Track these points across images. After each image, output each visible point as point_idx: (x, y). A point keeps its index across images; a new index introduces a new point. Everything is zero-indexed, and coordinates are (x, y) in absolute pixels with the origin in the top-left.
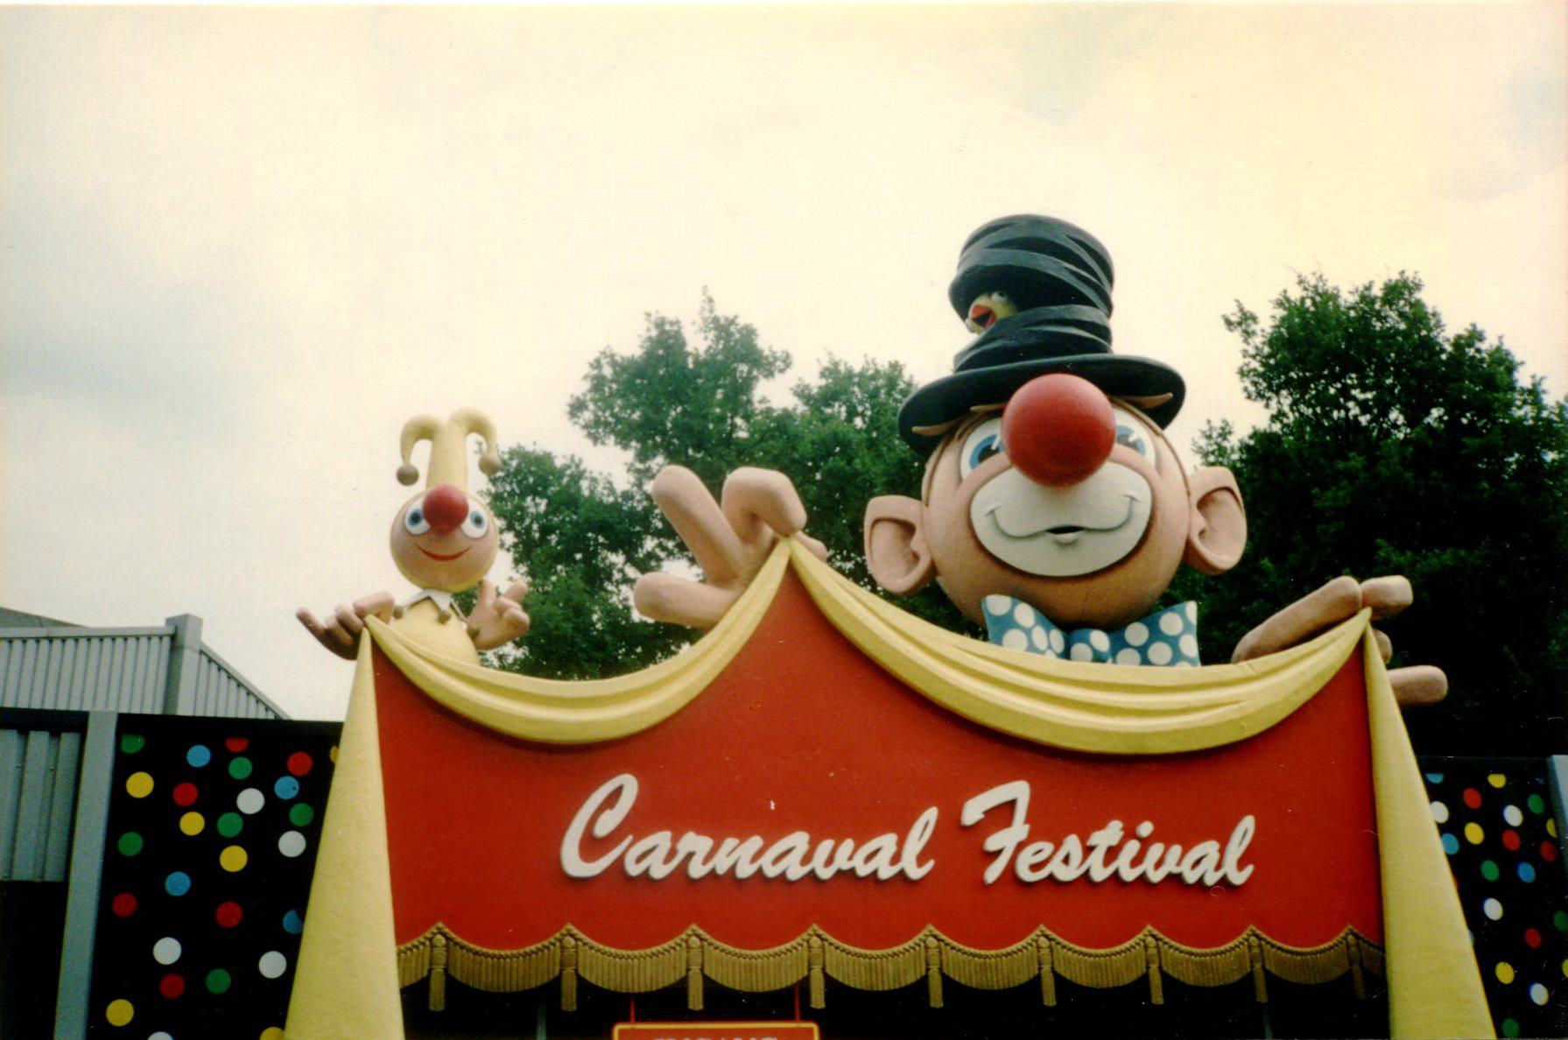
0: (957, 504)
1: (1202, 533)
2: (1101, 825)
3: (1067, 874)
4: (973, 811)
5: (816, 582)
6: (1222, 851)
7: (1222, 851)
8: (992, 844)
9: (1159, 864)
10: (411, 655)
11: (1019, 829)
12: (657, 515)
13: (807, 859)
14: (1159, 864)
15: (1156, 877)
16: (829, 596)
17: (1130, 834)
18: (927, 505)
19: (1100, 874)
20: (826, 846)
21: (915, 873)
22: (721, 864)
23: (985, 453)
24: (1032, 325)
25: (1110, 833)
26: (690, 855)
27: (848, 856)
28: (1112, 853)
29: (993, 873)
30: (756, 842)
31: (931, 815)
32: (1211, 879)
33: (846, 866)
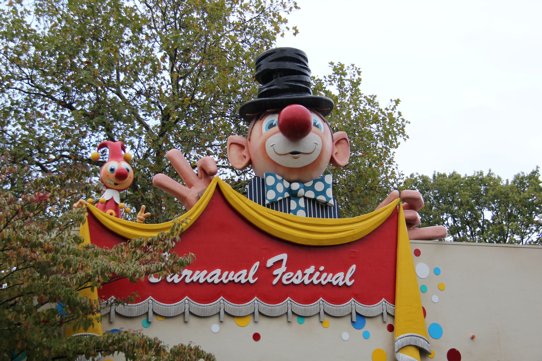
0: (260, 142)
1: (336, 153)
2: (308, 267)
3: (297, 282)
4: (270, 263)
5: (225, 191)
6: (345, 276)
7: (345, 276)
8: (275, 273)
9: (325, 279)
10: (102, 216)
11: (283, 268)
12: (158, 101)
13: (220, 277)
14: (325, 279)
15: (324, 283)
16: (229, 196)
17: (317, 270)
18: (249, 140)
19: (307, 282)
20: (226, 273)
21: (252, 281)
22: (195, 278)
23: (271, 126)
24: (287, 81)
25: (312, 269)
26: (186, 276)
27: (233, 276)
28: (311, 275)
29: (275, 282)
30: (205, 272)
31: (257, 264)
32: (341, 284)
33: (232, 279)
